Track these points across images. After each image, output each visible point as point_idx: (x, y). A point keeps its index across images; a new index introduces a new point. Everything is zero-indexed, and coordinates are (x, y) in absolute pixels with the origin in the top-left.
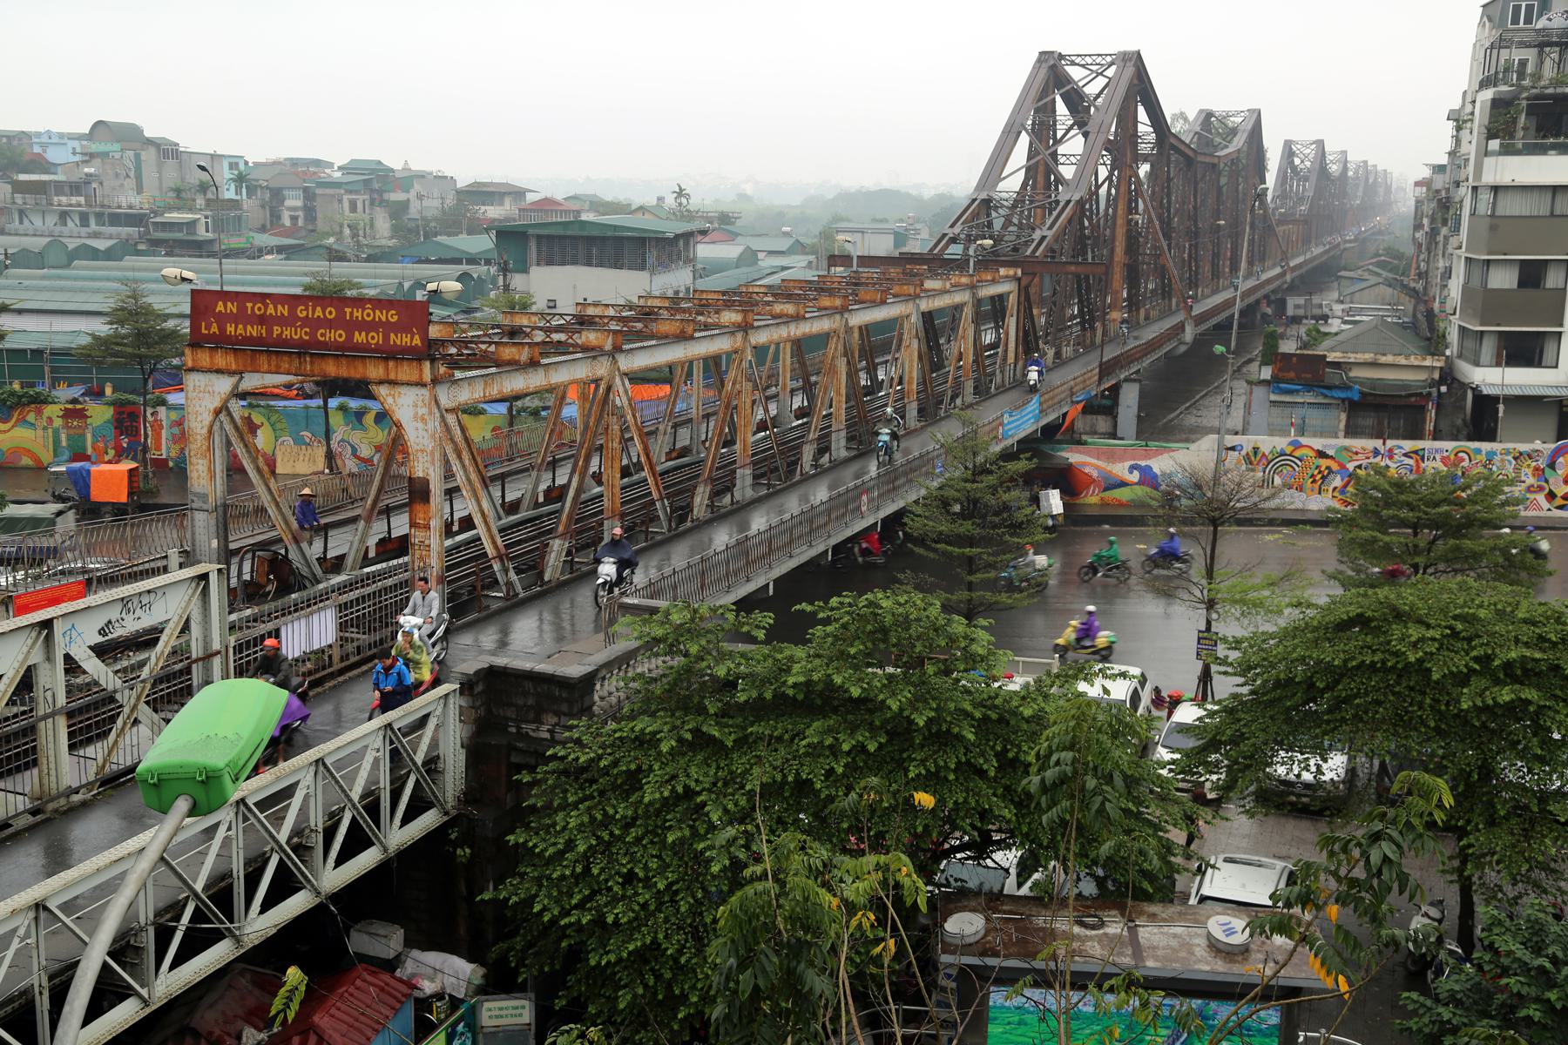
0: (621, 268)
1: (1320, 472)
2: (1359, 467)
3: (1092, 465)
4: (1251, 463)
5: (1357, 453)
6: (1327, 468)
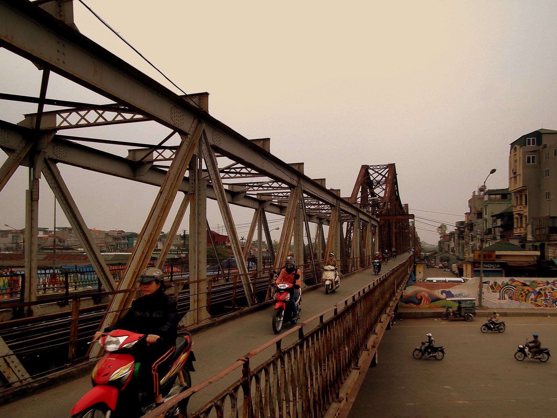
0: (80, 378)
1: (525, 292)
2: (541, 289)
3: (425, 291)
4: (494, 289)
5: (539, 284)
6: (527, 290)
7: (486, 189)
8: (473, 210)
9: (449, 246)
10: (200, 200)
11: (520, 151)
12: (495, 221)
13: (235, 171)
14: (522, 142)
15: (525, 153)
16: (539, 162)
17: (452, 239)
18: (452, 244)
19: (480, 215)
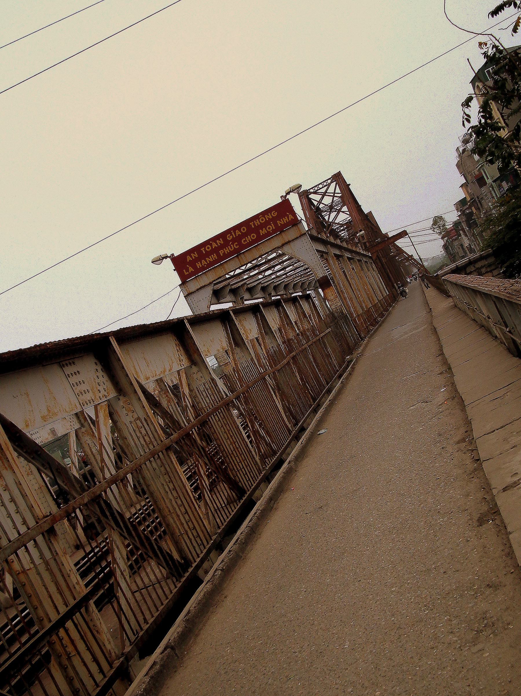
8: (469, 178)
9: (462, 245)
12: (500, 186)
13: (229, 276)
17: (461, 232)
18: (466, 242)
19: (481, 181)
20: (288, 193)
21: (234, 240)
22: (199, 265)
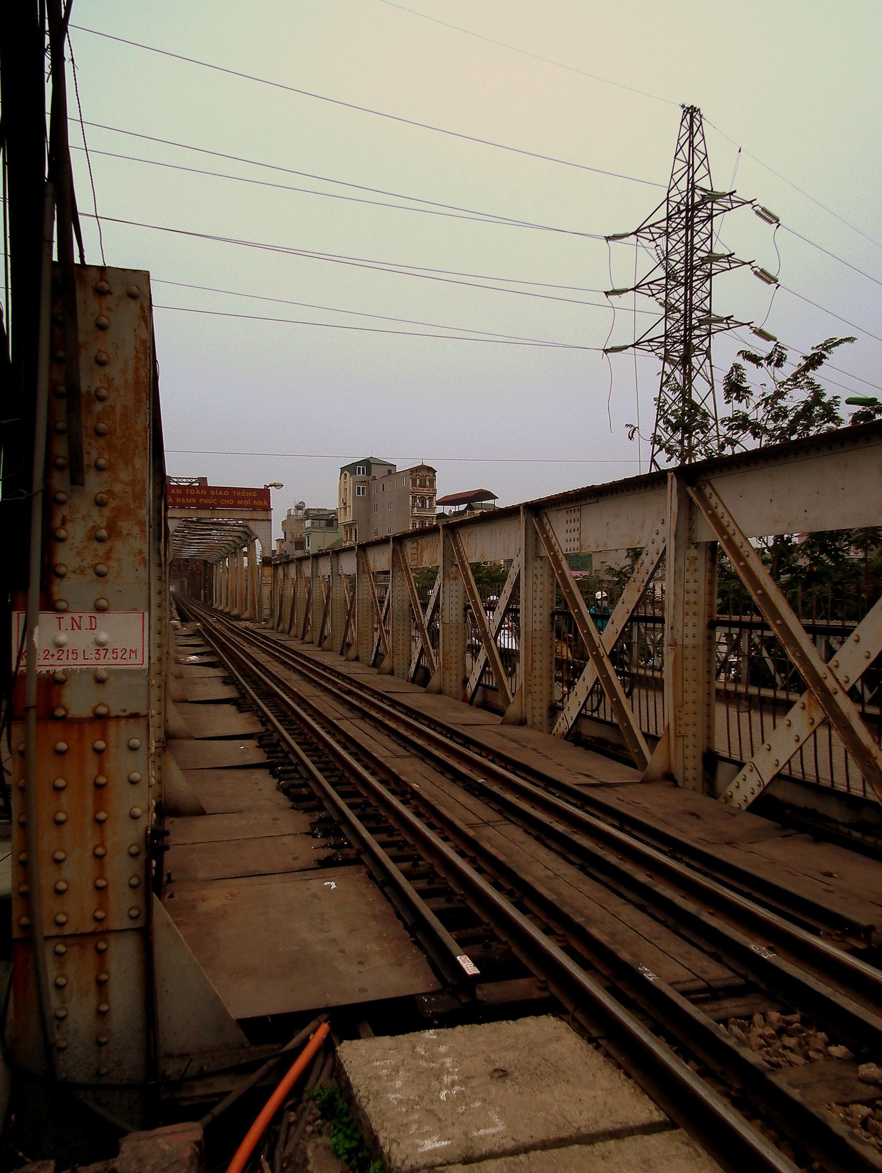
7: (304, 507)
8: (289, 537)
10: (686, 669)
11: (350, 480)
14: (349, 470)
15: (355, 483)
16: (369, 495)
20: (271, 486)
21: (215, 497)
22: (178, 500)
